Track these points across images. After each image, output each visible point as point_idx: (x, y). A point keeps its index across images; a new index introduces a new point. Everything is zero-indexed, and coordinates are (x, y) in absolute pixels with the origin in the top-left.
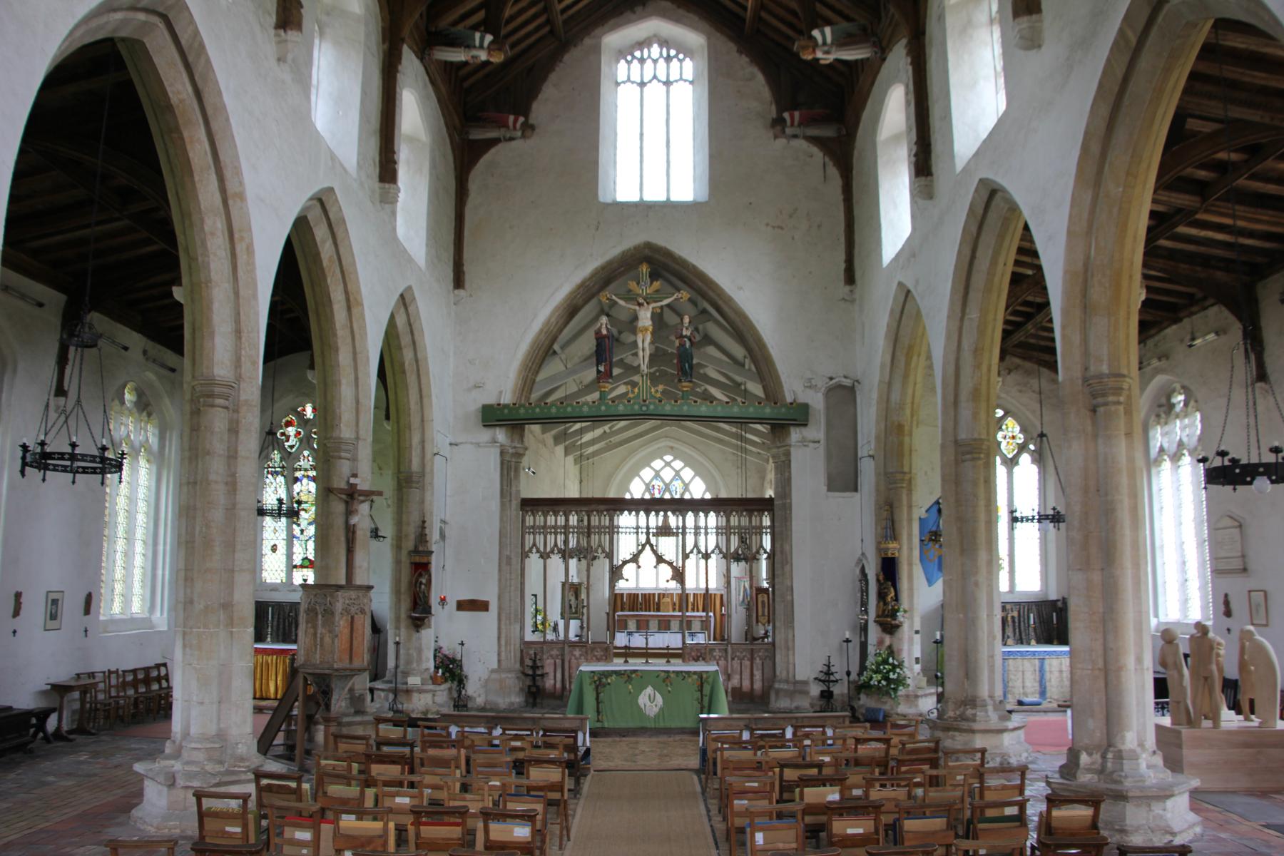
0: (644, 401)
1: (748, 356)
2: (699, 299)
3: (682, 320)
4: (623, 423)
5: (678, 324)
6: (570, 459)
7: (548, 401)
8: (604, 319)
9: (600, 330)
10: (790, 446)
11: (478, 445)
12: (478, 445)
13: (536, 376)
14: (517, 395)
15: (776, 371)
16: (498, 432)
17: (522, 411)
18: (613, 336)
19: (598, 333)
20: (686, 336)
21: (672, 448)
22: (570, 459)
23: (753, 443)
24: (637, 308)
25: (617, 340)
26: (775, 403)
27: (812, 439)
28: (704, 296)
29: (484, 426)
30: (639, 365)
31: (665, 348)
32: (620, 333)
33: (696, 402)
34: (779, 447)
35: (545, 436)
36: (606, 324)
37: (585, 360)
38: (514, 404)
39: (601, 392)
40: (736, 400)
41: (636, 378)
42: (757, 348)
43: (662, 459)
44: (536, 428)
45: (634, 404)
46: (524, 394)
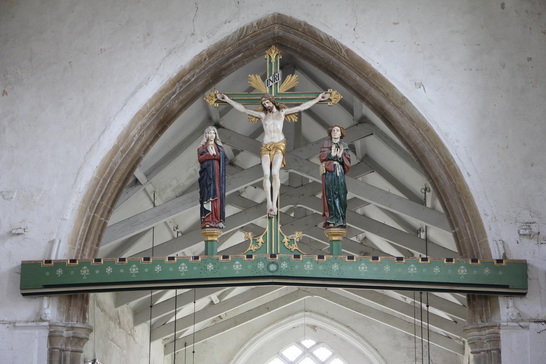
0: (273, 256)
1: (429, 186)
2: (357, 101)
3: (330, 134)
4: (238, 290)
5: (324, 139)
6: (158, 345)
7: (126, 255)
8: (212, 132)
9: (205, 147)
10: (499, 327)
11: (13, 324)
12: (13, 324)
13: (107, 218)
14: (77, 246)
15: (474, 210)
16: (45, 306)
17: (85, 271)
18: (225, 158)
19: (203, 152)
20: (336, 158)
21: (314, 327)
22: (158, 345)
23: (440, 322)
24: (262, 115)
25: (232, 164)
26: (474, 261)
27: (534, 316)
28: (363, 96)
29: (24, 295)
30: (265, 202)
31: (305, 175)
32: (236, 152)
33: (351, 258)
34: (480, 329)
35: (119, 309)
36: (215, 140)
37: (183, 193)
38: (73, 261)
39: (207, 242)
40: (413, 255)
41: (261, 221)
42: (444, 176)
43: (299, 344)
44: (106, 298)
45: (258, 260)
46: (89, 244)
